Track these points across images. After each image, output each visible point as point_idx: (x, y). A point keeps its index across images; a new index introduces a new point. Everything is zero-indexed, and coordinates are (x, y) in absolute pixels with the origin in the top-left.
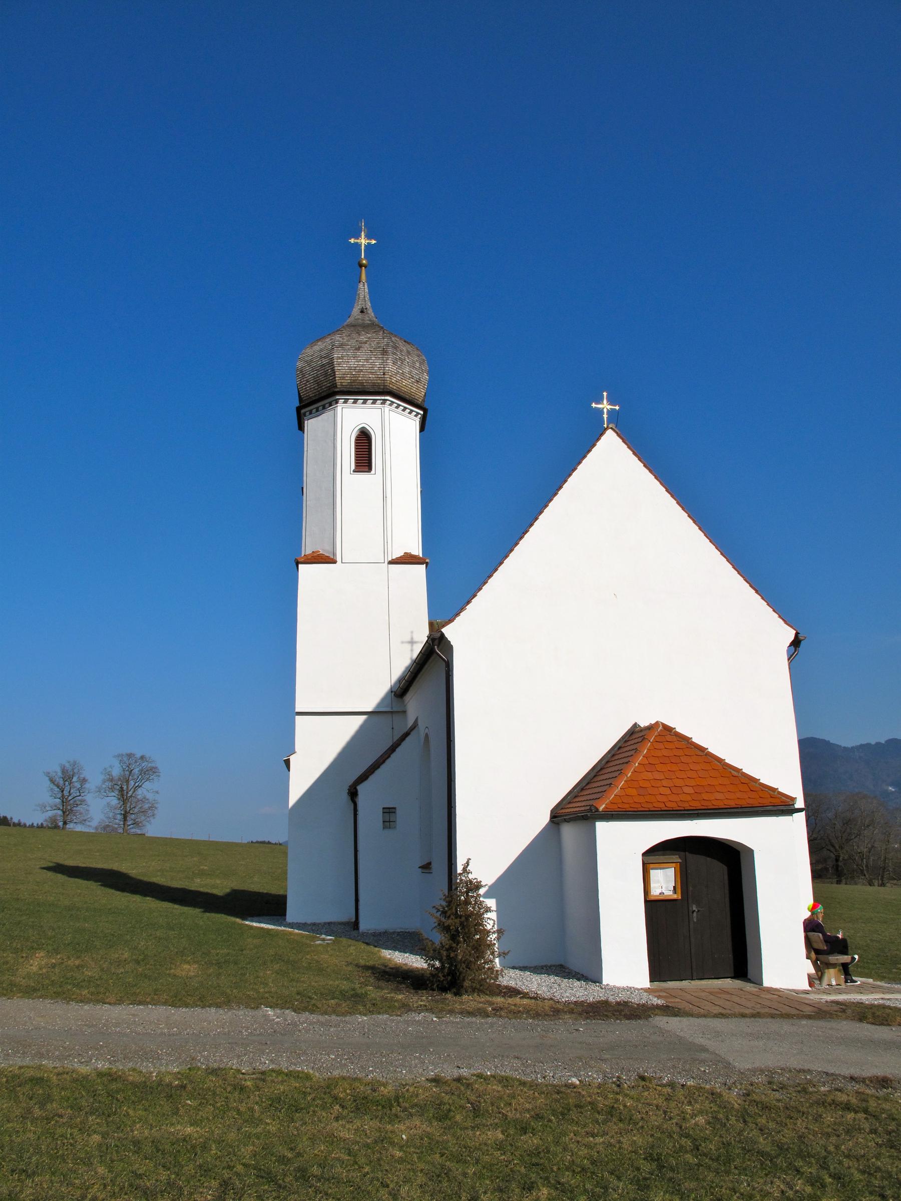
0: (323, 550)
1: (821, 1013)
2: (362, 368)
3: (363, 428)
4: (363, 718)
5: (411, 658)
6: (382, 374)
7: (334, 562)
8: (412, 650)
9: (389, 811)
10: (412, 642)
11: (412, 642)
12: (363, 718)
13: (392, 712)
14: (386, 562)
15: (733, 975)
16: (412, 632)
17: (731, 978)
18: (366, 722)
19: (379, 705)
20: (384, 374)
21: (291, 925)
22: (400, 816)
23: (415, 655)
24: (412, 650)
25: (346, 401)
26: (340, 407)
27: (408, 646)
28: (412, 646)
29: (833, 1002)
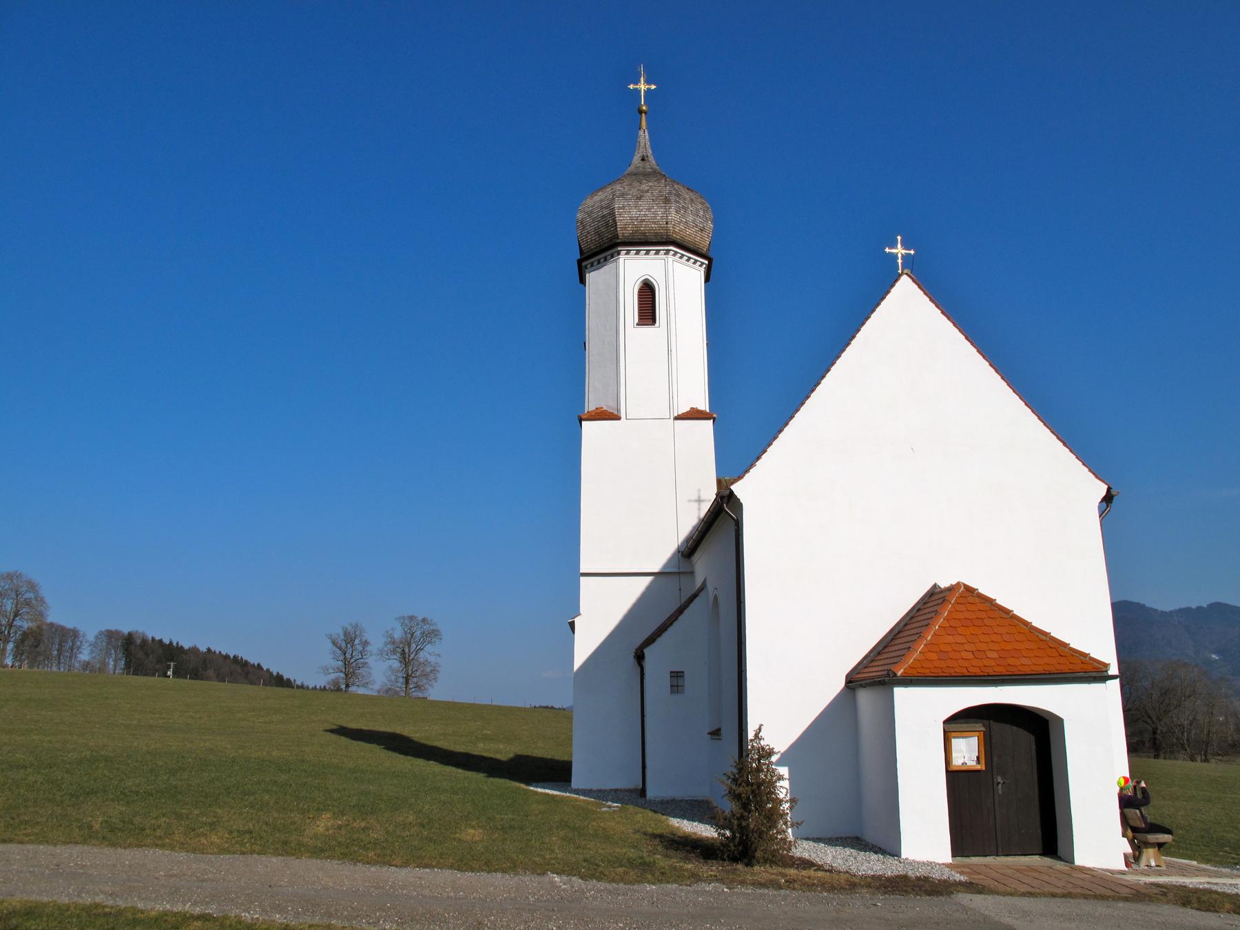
0: (607, 405)
1: (1139, 895)
2: (644, 218)
3: (647, 279)
4: (649, 579)
5: (699, 518)
6: (665, 223)
7: (618, 418)
8: (699, 509)
9: (677, 675)
10: (699, 501)
11: (699, 501)
12: (649, 579)
13: (679, 573)
14: (672, 418)
15: (1041, 852)
16: (699, 490)
17: (1040, 855)
18: (652, 583)
19: (666, 566)
20: (667, 223)
21: (577, 792)
22: (688, 681)
23: (703, 514)
24: (699, 509)
25: (628, 252)
26: (622, 258)
27: (696, 505)
28: (699, 504)
29: (1152, 884)
